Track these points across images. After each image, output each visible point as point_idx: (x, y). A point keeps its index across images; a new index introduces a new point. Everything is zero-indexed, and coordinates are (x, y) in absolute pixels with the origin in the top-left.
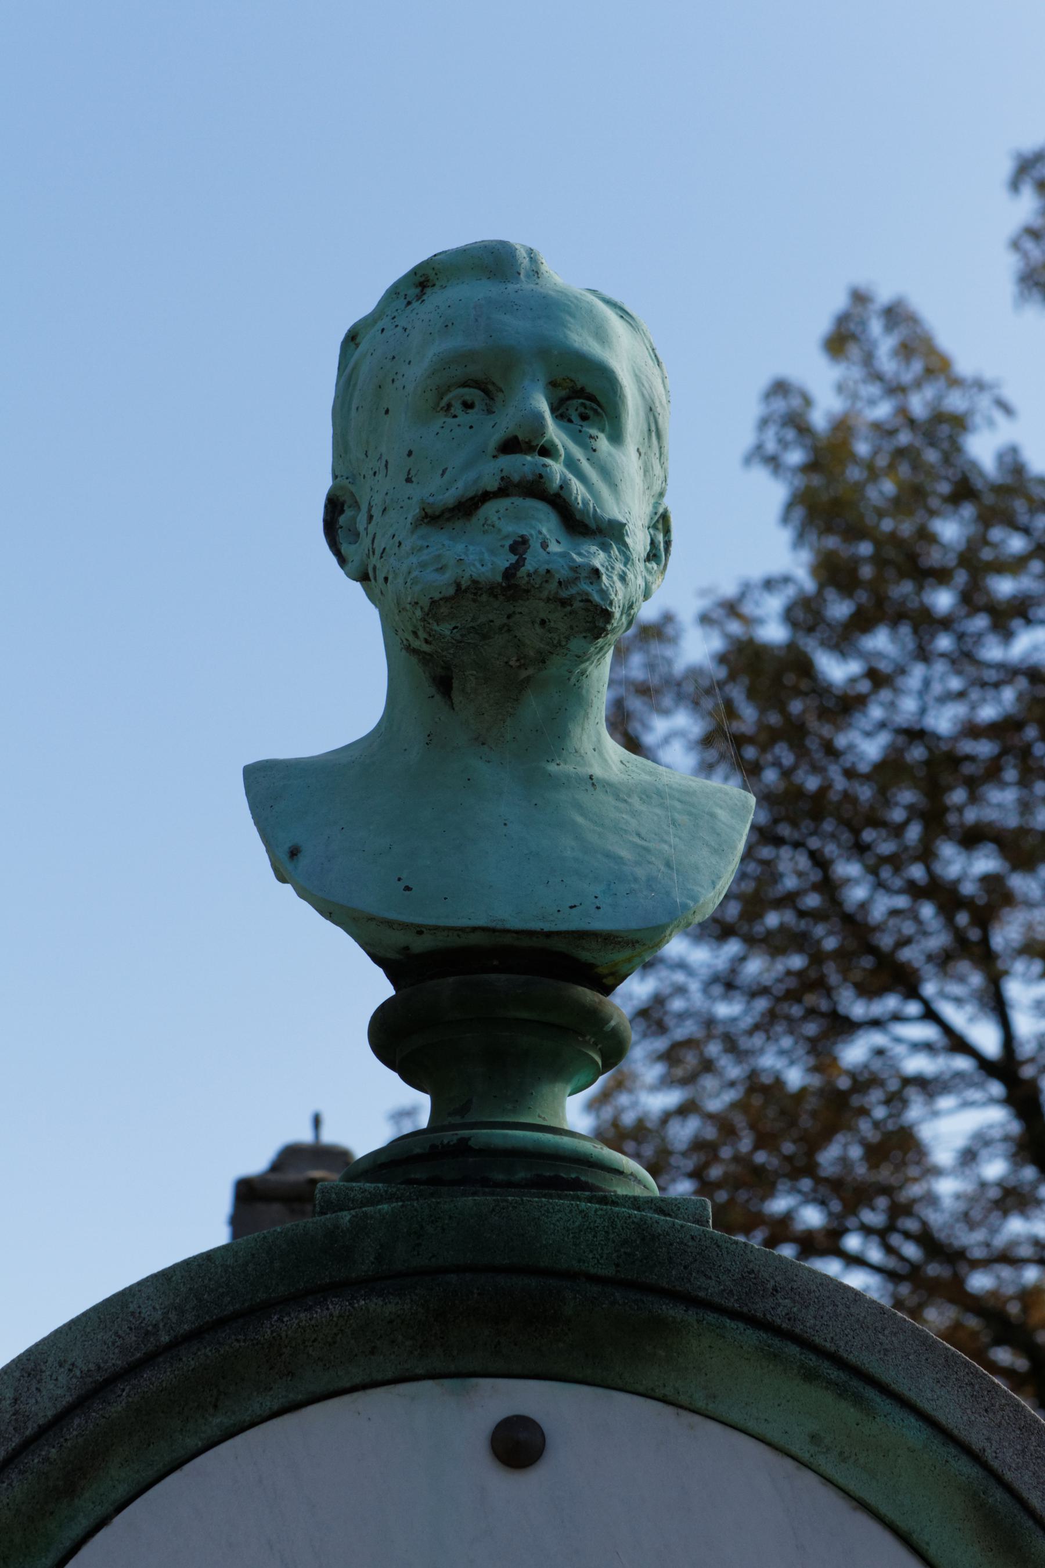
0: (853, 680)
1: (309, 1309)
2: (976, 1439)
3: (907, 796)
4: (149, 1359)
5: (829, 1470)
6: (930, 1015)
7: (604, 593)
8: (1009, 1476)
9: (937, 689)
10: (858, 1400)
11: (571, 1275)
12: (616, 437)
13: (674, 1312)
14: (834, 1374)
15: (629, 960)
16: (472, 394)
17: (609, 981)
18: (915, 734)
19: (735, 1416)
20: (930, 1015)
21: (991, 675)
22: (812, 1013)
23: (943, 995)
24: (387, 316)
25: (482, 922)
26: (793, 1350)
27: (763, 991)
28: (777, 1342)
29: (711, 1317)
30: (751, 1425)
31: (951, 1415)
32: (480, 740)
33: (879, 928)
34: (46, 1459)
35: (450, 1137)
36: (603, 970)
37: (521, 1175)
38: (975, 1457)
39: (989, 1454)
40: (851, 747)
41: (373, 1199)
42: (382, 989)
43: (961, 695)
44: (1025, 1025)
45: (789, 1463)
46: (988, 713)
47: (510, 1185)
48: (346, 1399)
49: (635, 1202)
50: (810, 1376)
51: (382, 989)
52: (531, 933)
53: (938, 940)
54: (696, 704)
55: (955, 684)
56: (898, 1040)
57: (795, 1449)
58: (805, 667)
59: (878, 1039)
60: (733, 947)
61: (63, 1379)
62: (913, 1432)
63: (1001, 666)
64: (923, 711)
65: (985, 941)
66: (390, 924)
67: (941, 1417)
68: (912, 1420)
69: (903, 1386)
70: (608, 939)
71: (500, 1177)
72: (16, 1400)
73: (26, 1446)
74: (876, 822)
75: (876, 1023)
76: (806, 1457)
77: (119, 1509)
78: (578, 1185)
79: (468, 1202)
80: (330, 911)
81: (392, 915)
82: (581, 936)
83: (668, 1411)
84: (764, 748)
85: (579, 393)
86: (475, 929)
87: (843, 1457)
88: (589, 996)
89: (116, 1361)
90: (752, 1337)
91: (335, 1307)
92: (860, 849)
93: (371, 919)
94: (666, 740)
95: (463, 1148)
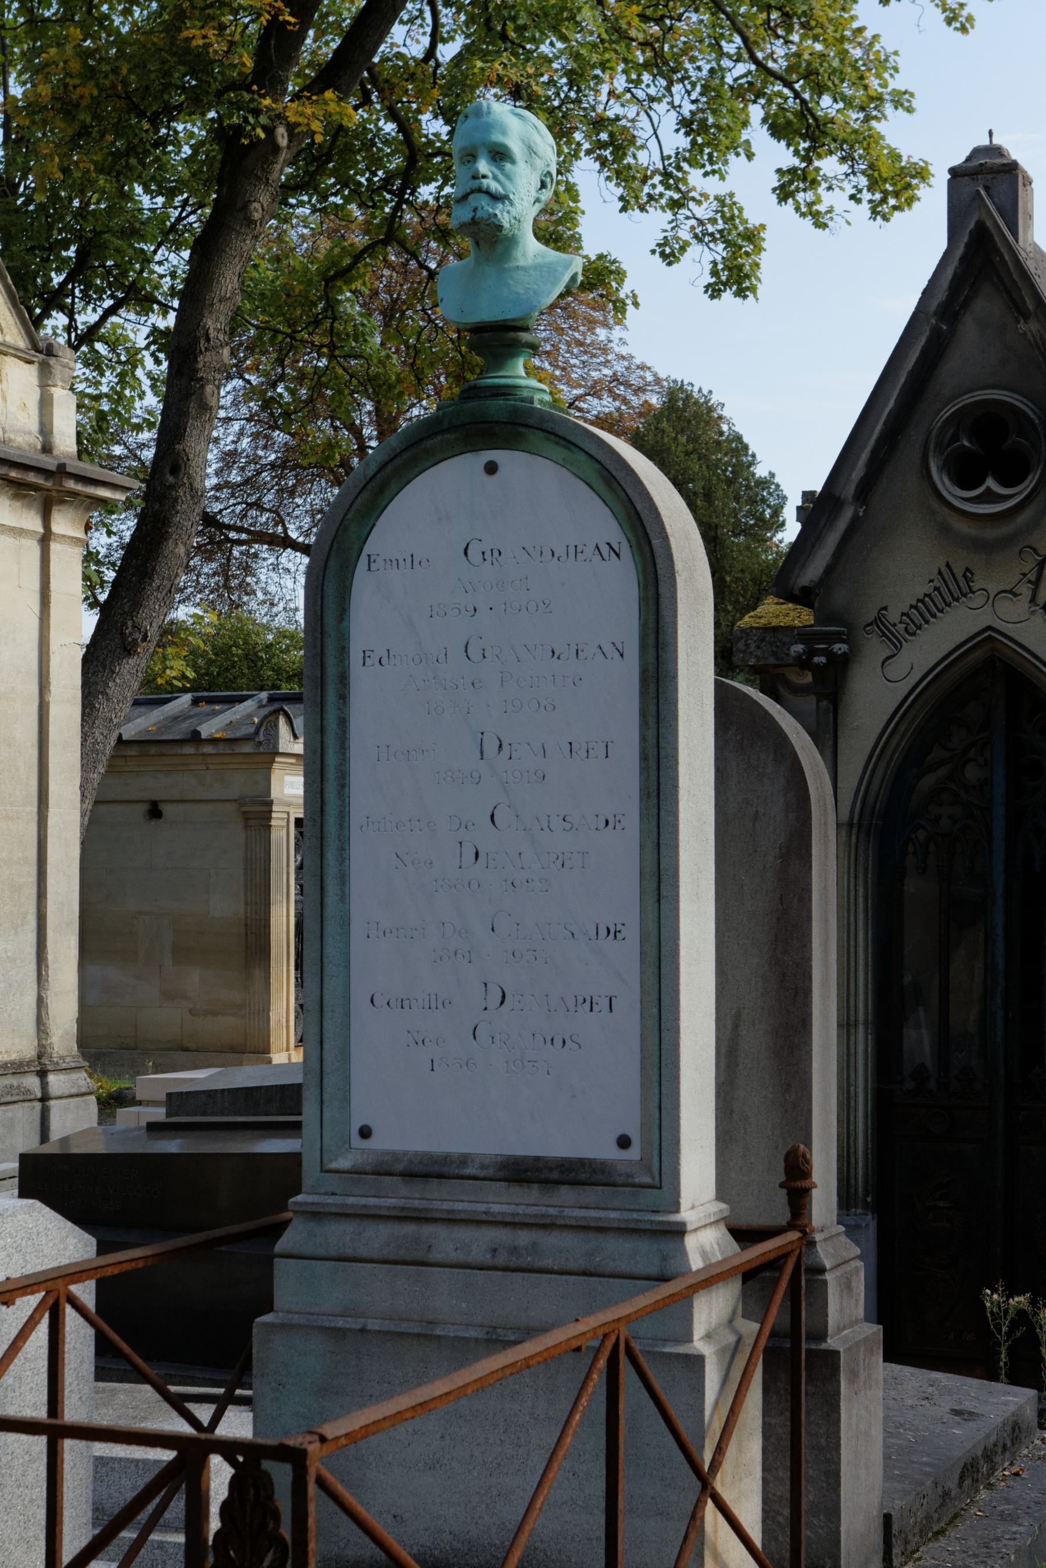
2: (599, 457)
4: (395, 457)
7: (499, 220)
10: (569, 449)
11: (496, 422)
12: (513, 162)
13: (522, 430)
14: (563, 443)
16: (469, 158)
26: (552, 437)
31: (593, 452)
32: (487, 260)
37: (488, 394)
50: (557, 444)
62: (582, 457)
69: (581, 445)
73: (367, 483)
85: (498, 153)
89: (387, 458)
90: (542, 434)
91: (439, 438)
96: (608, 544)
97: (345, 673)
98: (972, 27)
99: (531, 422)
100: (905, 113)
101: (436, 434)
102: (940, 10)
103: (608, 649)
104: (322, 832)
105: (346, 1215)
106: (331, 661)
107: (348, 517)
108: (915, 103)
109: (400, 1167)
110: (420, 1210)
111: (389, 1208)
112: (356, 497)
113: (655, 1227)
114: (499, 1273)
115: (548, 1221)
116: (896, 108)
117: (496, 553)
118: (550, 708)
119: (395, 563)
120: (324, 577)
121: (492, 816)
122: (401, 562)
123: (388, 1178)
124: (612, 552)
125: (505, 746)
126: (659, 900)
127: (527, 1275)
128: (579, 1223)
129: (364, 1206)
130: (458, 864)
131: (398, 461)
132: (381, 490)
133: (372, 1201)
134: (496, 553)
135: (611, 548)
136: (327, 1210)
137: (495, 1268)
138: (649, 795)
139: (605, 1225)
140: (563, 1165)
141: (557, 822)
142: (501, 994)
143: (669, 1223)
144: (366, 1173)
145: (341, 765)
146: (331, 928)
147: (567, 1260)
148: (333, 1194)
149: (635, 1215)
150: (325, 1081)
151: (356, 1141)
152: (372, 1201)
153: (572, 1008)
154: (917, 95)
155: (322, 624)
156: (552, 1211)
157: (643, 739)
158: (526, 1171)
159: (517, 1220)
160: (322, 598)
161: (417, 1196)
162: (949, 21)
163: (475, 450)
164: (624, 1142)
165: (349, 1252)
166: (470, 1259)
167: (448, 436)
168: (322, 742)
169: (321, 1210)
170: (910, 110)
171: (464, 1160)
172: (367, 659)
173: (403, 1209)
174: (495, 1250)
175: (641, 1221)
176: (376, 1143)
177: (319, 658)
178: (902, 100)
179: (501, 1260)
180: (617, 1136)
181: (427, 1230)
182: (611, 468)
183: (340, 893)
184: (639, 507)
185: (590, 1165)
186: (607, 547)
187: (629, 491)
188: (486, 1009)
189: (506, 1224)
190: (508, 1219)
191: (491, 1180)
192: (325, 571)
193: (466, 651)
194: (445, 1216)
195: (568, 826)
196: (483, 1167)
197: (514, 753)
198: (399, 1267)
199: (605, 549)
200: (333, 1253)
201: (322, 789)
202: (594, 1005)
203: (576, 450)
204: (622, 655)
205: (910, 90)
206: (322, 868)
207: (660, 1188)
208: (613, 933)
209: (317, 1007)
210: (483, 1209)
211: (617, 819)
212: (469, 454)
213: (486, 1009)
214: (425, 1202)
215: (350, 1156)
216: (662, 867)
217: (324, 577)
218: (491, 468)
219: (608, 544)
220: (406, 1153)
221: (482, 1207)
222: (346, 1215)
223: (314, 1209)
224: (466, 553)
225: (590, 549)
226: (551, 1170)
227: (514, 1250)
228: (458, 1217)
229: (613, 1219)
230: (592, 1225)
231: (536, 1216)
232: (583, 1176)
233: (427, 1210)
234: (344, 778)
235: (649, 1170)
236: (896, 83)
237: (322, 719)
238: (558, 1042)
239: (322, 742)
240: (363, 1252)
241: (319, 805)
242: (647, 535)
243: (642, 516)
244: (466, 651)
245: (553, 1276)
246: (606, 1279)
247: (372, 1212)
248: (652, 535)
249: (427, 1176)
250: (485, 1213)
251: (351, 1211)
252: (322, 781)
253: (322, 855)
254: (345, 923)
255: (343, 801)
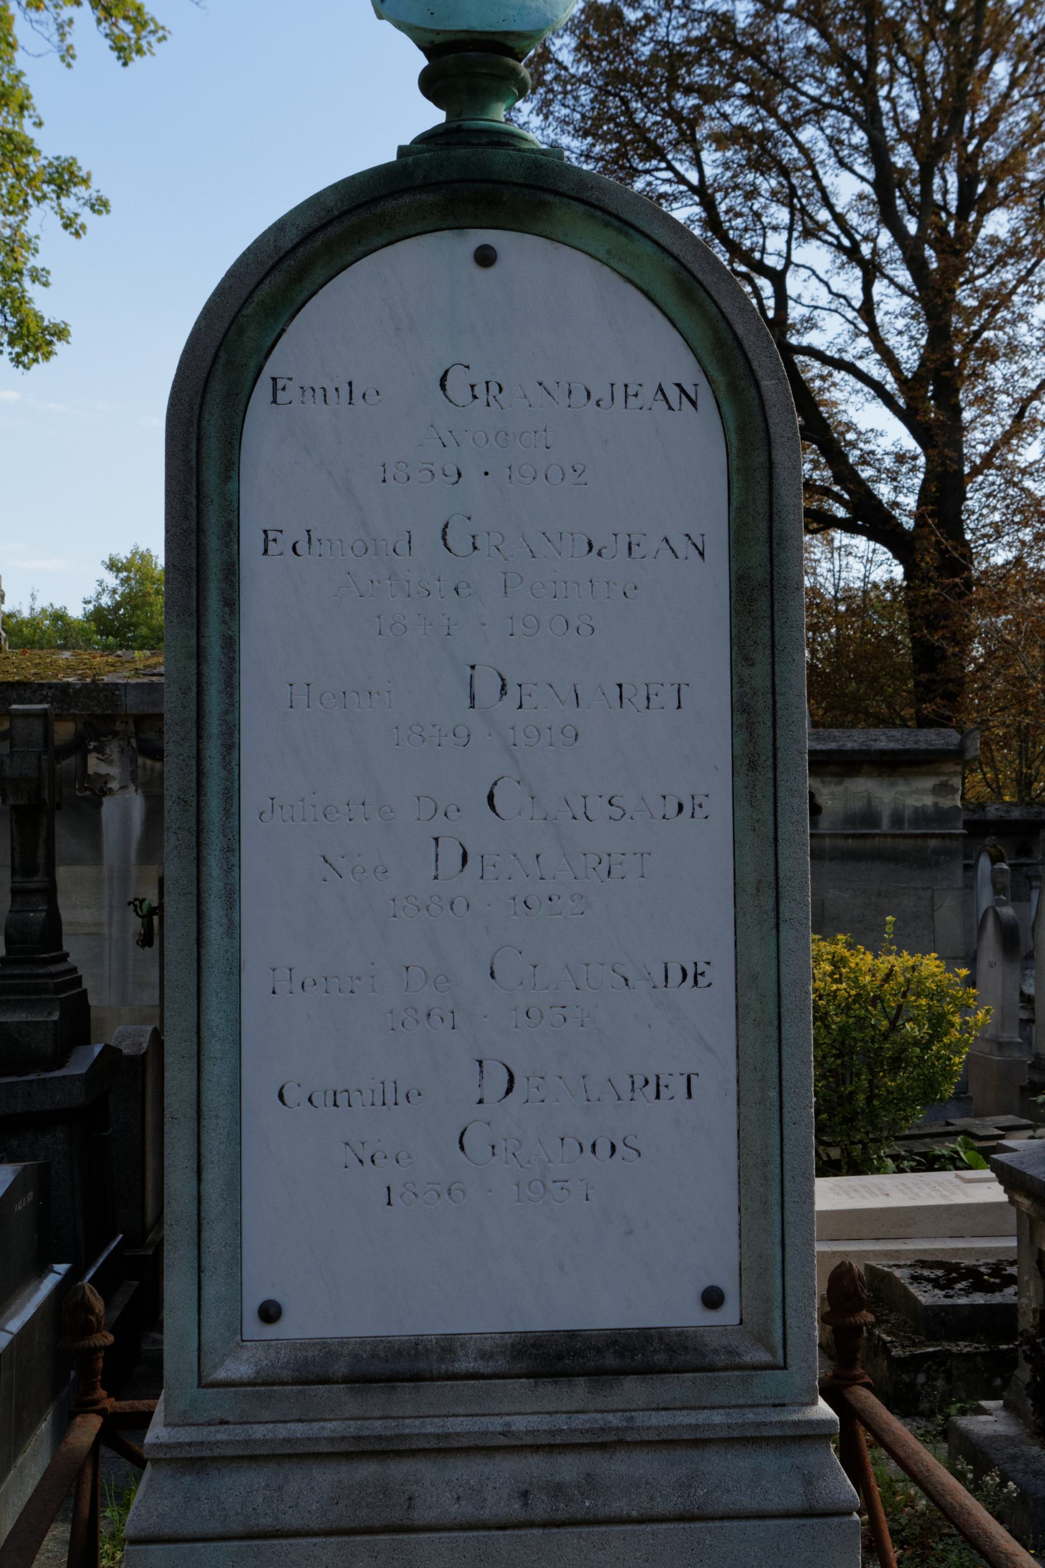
0: (637, 20)
1: (396, 199)
2: (676, 250)
3: (660, 71)
4: (330, 222)
5: (615, 265)
6: (670, 168)
8: (689, 266)
9: (674, 23)
10: (627, 235)
13: (549, 198)
14: (616, 223)
15: (529, 45)
17: (520, 56)
18: (666, 44)
19: (575, 243)
20: (670, 168)
21: (697, 15)
22: (622, 168)
23: (676, 159)
24: (647, 1082)
25: (464, 28)
26: (599, 213)
27: (602, 158)
28: (592, 210)
29: (565, 200)
30: (582, 246)
33: (649, 130)
34: (289, 266)
35: (454, 125)
36: (517, 51)
37: (484, 140)
38: (676, 258)
39: (681, 256)
40: (637, 50)
41: (421, 152)
42: (422, 62)
43: (684, 25)
44: (709, 171)
45: (598, 263)
46: (695, 33)
47: (479, 145)
48: (413, 239)
49: (532, 151)
50: (607, 225)
51: (422, 62)
52: (486, 33)
53: (674, 135)
54: (573, 32)
55: (682, 21)
56: (657, 179)
57: (600, 257)
58: (620, 15)
59: (649, 178)
60: (590, 140)
61: (294, 231)
62: (649, 248)
63: (701, 12)
64: (668, 35)
65: (693, 134)
66: (425, 30)
67: (661, 241)
68: (649, 243)
70: (519, 35)
71: (475, 141)
72: (275, 241)
73: (280, 260)
74: (649, 84)
75: (648, 172)
76: (605, 260)
77: (321, 287)
78: (508, 144)
79: (461, 152)
80: (400, 26)
81: (426, 26)
82: (507, 34)
83: (548, 242)
84: (601, 51)
86: (462, 31)
87: (620, 260)
88: (512, 62)
90: (581, 208)
91: (407, 198)
92: (641, 96)
93: (417, 28)
94: (560, 49)
95: (459, 130)
96: (679, 385)
97: (233, 564)
98: (85, 233)
99: (564, 187)
100: (41, 287)
101: (407, 190)
102: (58, 217)
103: (679, 543)
104: (199, 821)
105: (253, 1458)
106: (213, 542)
107: (245, 312)
108: (51, 279)
109: (341, 1368)
110: (389, 1439)
111: (331, 1440)
112: (261, 282)
113: (789, 1432)
114: (537, 1532)
115: (612, 1437)
116: (33, 282)
117: (494, 389)
118: (585, 630)
119: (319, 393)
120: (201, 406)
121: (491, 797)
122: (331, 393)
123: (322, 1388)
124: (684, 398)
125: (512, 688)
126: (777, 926)
127: (584, 1530)
128: (664, 1436)
129: (288, 1440)
130: (433, 874)
131: (336, 229)
132: (300, 275)
133: (298, 1430)
134: (494, 389)
135: (683, 391)
136: (217, 1452)
137: (531, 1524)
138: (753, 766)
139: (707, 1435)
140: (616, 1342)
141: (598, 808)
142: (506, 1077)
143: (797, 1424)
144: (282, 1383)
145: (226, 712)
146: (214, 981)
147: (652, 1499)
148: (222, 1422)
149: (750, 1416)
150: (205, 1235)
151: (253, 1328)
152: (298, 1430)
153: (626, 1094)
154: (52, 273)
155: (199, 483)
156: (614, 1420)
157: (737, 680)
158: (560, 1357)
159: (558, 1441)
160: (199, 440)
161: (377, 1413)
162: (66, 226)
163: (460, 226)
164: (712, 1299)
165: (266, 1523)
166: (486, 1514)
167: (424, 198)
168: (199, 675)
169: (207, 1453)
170: (46, 284)
171: (448, 1345)
172: (271, 544)
173: (358, 1438)
174: (525, 1494)
175: (765, 1424)
176: (288, 1329)
177: (193, 537)
178: (39, 276)
179: (540, 1509)
180: (701, 1289)
181: (398, 1470)
182: (694, 267)
183: (225, 921)
184: (740, 329)
185: (661, 1338)
186: (677, 390)
187: (724, 305)
188: (481, 1102)
189: (536, 1448)
190: (543, 1440)
191: (504, 1377)
192: (203, 397)
193: (444, 539)
194: (433, 1444)
195: (617, 813)
196: (484, 1355)
197: (525, 698)
198: (358, 1538)
199: (673, 394)
200: (236, 1526)
201: (199, 751)
202: (662, 1089)
203: (636, 236)
204: (702, 554)
205: (47, 268)
206: (198, 881)
207: (785, 1367)
208: (692, 976)
209: (192, 1112)
210: (499, 1429)
211: (697, 802)
212: (447, 233)
213: (481, 1102)
214: (392, 1423)
215: (245, 1355)
216: (781, 875)
217: (201, 406)
218: (485, 257)
219: (679, 385)
220: (343, 1341)
221: (495, 1424)
222: (253, 1458)
223: (194, 1453)
224: (443, 386)
225: (649, 392)
226: (599, 1351)
227: (557, 1490)
228: (455, 1444)
229: (719, 1425)
230: (686, 1436)
231: (591, 1431)
232: (660, 1358)
233: (401, 1437)
234: (231, 735)
235: (762, 1340)
236: (35, 262)
237: (199, 636)
238: (603, 1149)
239: (199, 675)
240: (292, 1520)
241: (194, 776)
242: (752, 373)
243: (746, 343)
244: (444, 539)
245: (629, 1527)
246: (717, 1524)
247: (301, 1450)
248: (760, 373)
249: (393, 1379)
250: (503, 1434)
251: (264, 1451)
252: (199, 738)
253: (199, 861)
254: (235, 970)
255: (230, 772)
